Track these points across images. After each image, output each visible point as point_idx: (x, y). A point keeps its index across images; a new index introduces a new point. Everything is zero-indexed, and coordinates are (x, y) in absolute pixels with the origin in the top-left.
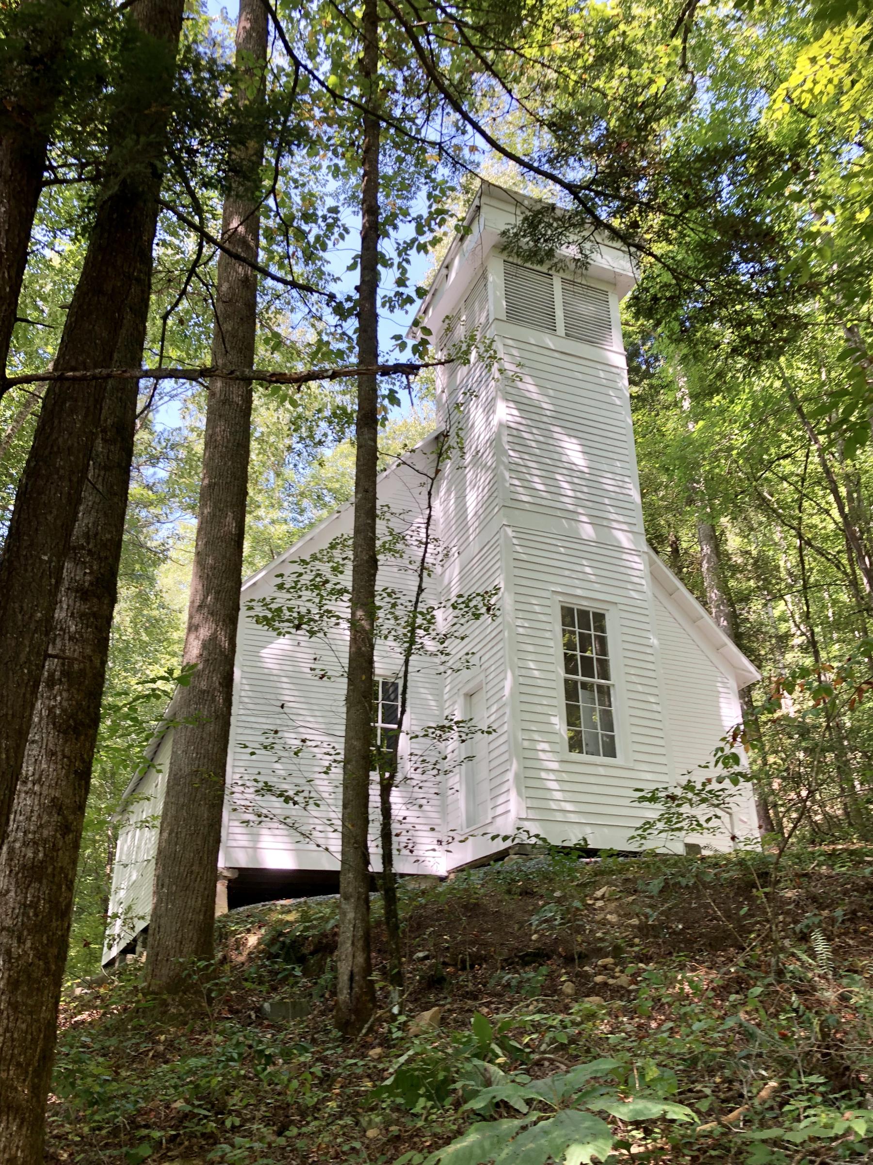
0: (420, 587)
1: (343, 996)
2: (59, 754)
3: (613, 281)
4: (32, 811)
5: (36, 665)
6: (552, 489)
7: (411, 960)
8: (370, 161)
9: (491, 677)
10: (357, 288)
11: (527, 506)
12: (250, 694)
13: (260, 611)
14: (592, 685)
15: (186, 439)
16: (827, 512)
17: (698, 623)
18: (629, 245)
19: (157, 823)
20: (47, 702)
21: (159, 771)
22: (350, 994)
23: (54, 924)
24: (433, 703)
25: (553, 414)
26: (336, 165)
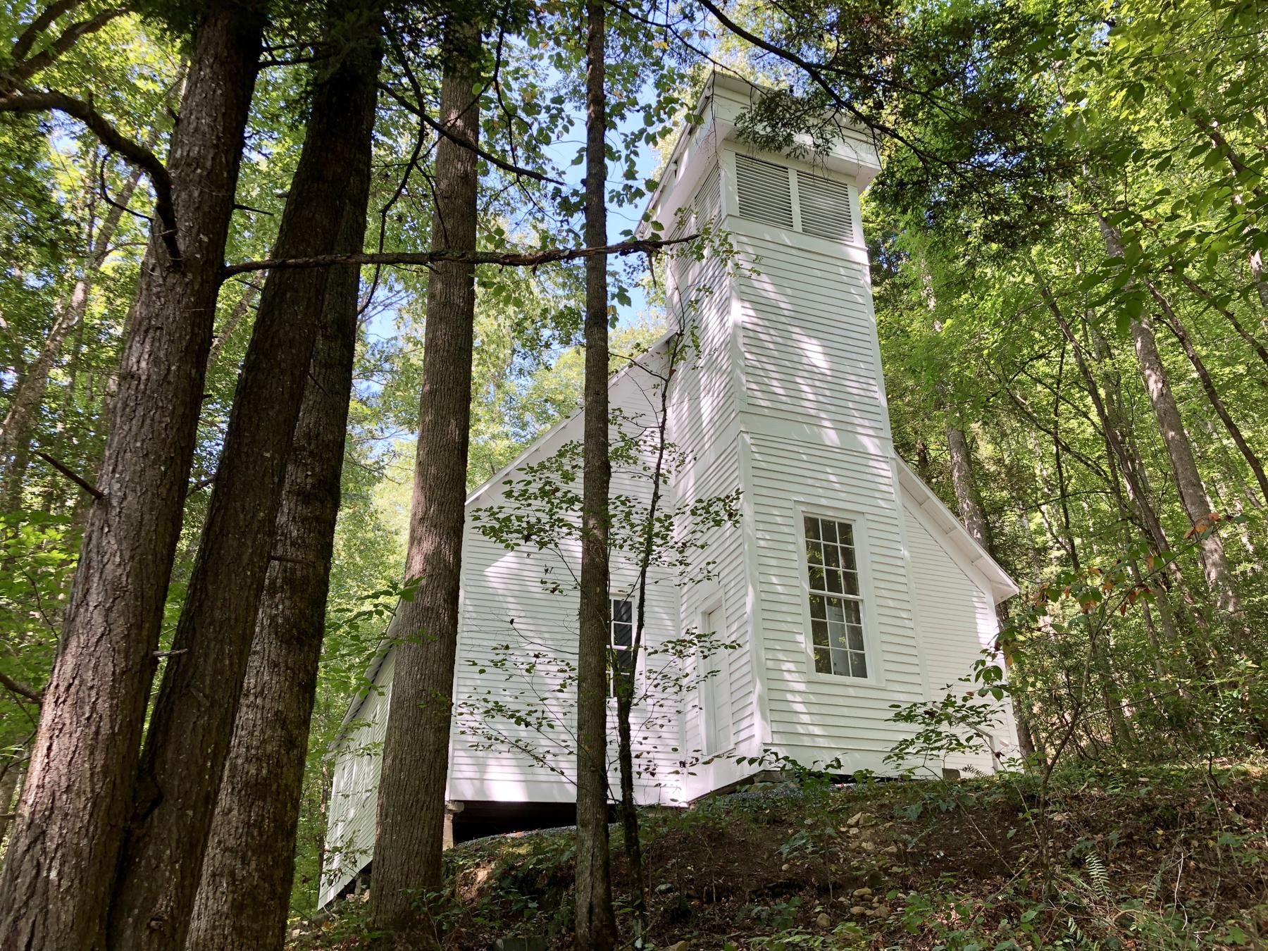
0: (656, 494)
1: (582, 930)
2: (282, 665)
3: (853, 174)
4: (254, 726)
5: (260, 567)
6: (792, 393)
7: (653, 893)
8: (594, 49)
9: (732, 592)
10: (584, 182)
11: (766, 412)
12: (474, 615)
13: (486, 521)
14: (839, 600)
15: (401, 350)
16: (1085, 415)
17: (951, 534)
18: (872, 127)
19: (380, 751)
20: (268, 610)
21: (382, 694)
22: (589, 928)
23: (280, 845)
24: (669, 623)
25: (792, 314)
26: (559, 55)
